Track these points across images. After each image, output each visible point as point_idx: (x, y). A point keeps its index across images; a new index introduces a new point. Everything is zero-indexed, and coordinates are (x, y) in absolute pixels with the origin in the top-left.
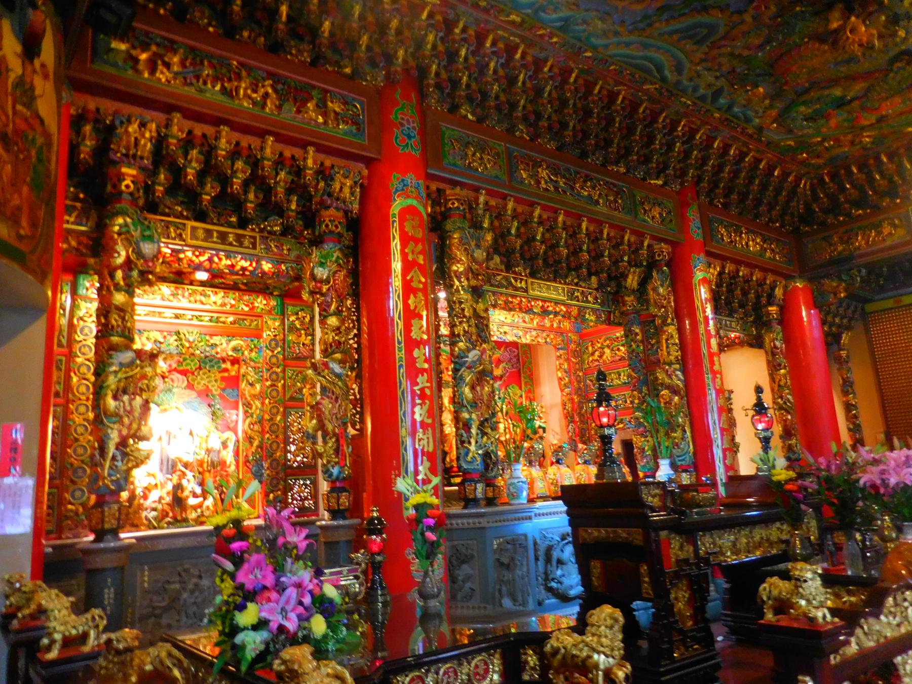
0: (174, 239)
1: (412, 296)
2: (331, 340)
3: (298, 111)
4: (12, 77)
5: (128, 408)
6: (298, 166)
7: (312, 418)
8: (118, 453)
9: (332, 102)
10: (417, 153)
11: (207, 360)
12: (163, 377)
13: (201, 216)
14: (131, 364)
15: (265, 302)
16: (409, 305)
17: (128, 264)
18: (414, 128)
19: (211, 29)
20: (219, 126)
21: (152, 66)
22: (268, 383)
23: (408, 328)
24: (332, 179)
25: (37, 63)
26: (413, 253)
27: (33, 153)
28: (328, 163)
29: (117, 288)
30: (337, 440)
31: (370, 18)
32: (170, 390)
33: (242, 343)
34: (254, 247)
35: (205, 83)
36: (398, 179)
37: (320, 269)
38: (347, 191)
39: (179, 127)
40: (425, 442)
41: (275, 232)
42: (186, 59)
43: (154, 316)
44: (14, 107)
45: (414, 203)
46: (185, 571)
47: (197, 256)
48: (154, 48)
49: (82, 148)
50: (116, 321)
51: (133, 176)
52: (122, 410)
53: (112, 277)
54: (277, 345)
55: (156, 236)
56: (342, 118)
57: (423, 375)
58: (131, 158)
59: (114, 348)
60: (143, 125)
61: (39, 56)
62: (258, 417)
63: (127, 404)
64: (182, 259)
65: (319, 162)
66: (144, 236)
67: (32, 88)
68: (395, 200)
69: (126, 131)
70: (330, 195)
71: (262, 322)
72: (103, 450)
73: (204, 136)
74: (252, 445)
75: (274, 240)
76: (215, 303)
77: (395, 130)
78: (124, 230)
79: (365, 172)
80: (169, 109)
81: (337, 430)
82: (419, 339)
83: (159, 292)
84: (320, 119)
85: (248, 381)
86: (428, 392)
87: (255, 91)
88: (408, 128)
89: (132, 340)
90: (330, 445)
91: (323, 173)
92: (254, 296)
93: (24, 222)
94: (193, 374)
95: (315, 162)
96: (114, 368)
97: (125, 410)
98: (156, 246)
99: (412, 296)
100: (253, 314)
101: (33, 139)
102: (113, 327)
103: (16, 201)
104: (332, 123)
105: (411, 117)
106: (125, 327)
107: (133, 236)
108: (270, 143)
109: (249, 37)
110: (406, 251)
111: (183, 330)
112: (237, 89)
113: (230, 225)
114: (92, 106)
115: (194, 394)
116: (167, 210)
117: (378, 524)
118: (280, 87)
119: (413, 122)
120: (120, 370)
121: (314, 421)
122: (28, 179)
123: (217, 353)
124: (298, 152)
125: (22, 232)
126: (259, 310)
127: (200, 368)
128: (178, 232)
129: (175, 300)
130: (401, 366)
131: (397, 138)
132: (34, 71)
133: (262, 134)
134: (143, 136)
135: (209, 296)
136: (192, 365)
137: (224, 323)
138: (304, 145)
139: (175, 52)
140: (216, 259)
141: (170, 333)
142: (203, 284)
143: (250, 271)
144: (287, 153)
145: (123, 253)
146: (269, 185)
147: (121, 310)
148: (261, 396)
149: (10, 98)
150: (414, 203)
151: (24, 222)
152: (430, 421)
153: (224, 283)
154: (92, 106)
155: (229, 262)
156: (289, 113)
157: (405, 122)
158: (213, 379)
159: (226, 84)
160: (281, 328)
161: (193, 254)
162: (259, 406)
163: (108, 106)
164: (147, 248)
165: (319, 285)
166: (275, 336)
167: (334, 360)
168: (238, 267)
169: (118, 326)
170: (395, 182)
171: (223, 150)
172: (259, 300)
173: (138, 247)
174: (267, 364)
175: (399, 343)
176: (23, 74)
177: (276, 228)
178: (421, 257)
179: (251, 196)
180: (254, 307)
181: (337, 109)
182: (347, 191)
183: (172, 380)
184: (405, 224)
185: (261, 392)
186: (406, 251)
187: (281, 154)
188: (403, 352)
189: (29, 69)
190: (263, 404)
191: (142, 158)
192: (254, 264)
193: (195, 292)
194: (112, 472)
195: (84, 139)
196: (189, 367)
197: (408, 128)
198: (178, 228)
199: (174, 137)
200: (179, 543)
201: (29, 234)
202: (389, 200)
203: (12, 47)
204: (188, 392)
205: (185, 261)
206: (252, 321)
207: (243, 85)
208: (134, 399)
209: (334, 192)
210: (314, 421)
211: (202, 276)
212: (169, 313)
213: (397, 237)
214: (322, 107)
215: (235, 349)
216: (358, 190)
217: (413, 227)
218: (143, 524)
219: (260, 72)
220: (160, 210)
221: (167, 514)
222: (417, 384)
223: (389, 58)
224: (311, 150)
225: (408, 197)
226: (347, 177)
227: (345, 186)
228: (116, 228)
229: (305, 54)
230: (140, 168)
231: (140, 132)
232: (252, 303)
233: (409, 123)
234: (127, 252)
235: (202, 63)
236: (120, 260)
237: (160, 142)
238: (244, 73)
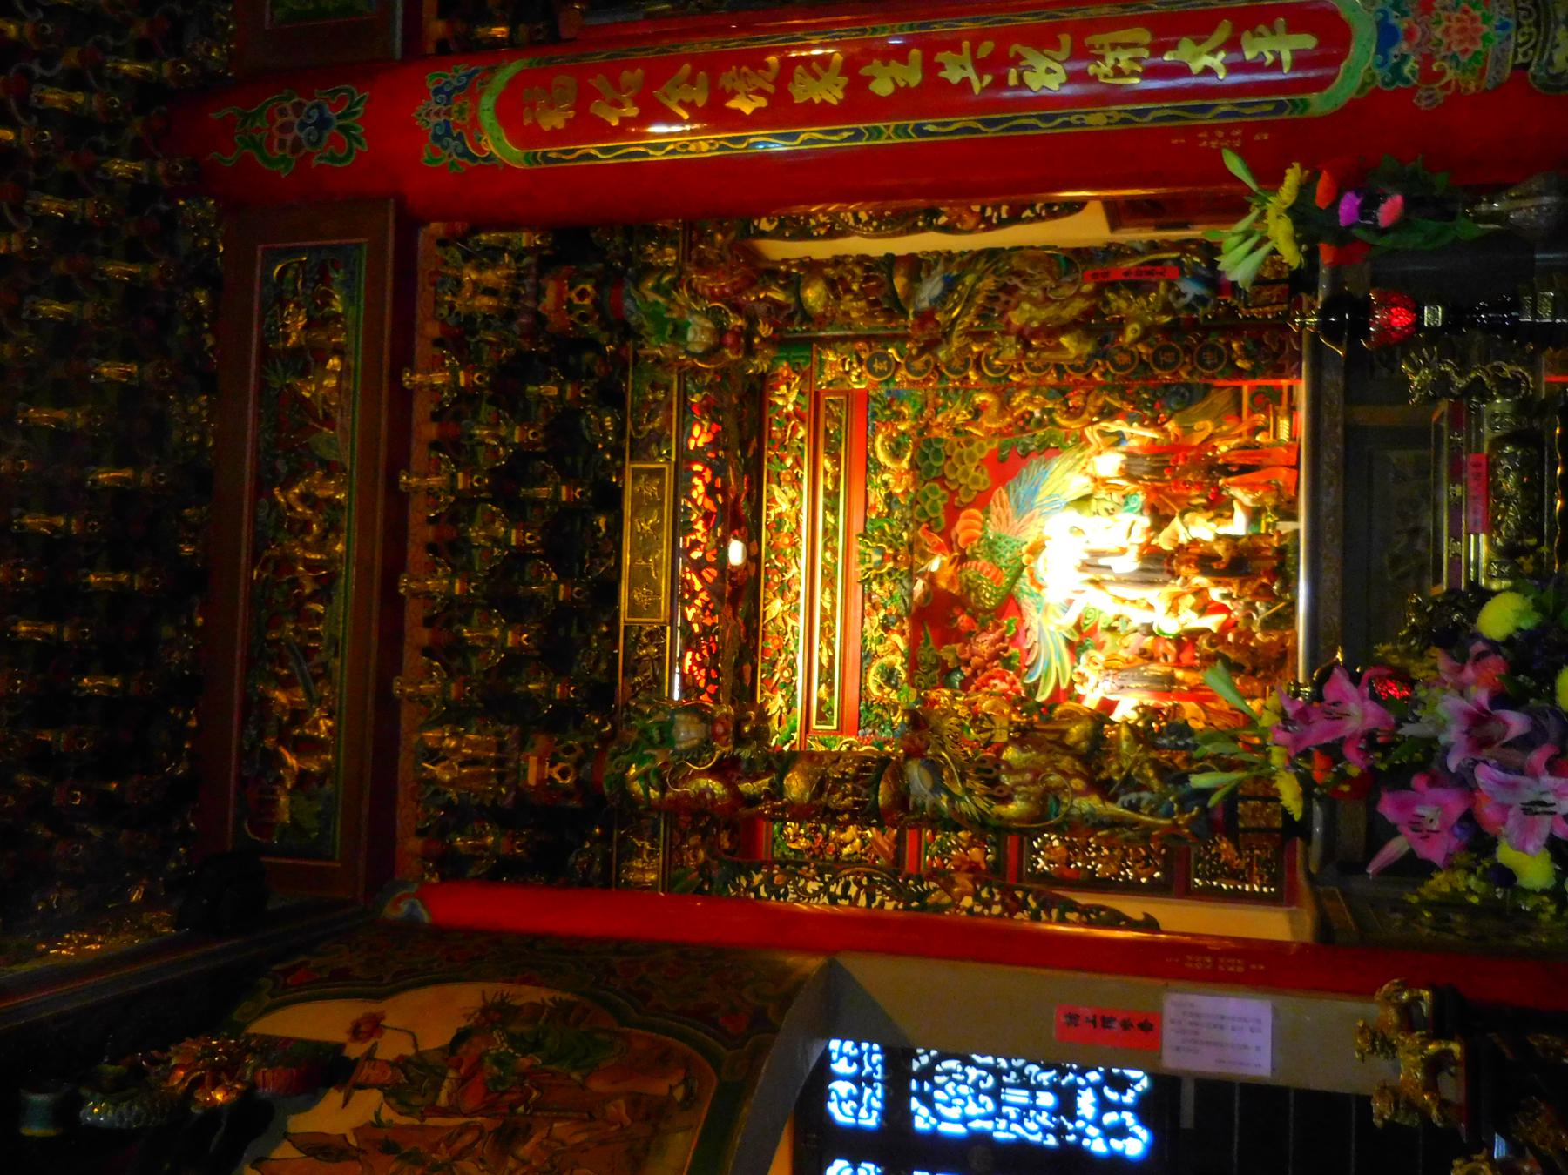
0: (662, 649)
1: (732, 104)
2: (862, 304)
3: (328, 421)
4: (388, 1114)
5: (1028, 776)
6: (455, 402)
7: (1060, 347)
8: (1123, 799)
9: (287, 337)
10: (360, 100)
11: (923, 465)
12: (963, 558)
13: (607, 591)
14: (934, 768)
15: (783, 388)
16: (757, 111)
17: (723, 770)
18: (298, 108)
19: (199, 621)
20: (402, 597)
21: (307, 746)
22: (972, 375)
23: (817, 114)
24: (470, 318)
25: (355, 1051)
26: (618, 104)
27: (524, 1062)
28: (433, 330)
29: (777, 791)
30: (1114, 287)
31: (71, 58)
32: (991, 545)
33: (880, 438)
34: (659, 473)
35: (315, 636)
36: (436, 152)
37: (690, 336)
38: (491, 277)
39: (421, 681)
40: (1124, 58)
41: (615, 423)
42: (276, 676)
43: (831, 630)
44: (444, 1112)
45: (488, 102)
46: (1396, 561)
47: (694, 595)
48: (269, 742)
49: (503, 851)
50: (844, 797)
51: (541, 762)
52: (1032, 789)
53: (753, 801)
54: (884, 357)
55: (660, 716)
56: (318, 308)
57: (941, 67)
58: (506, 768)
59: (902, 799)
60: (434, 755)
61: (341, 1047)
62: (1052, 399)
63: (1019, 779)
64: (703, 626)
65: (436, 351)
66: (662, 741)
67: (401, 1063)
68: (490, 157)
69: (452, 783)
70: (509, 316)
71: (829, 393)
72: (1114, 823)
73: (429, 622)
74: (1119, 410)
75: (636, 424)
76: (793, 502)
77: (315, 162)
78: (654, 781)
79: (437, 228)
80: (387, 705)
81: (1087, 288)
82: (844, 81)
83: (780, 622)
84: (334, 362)
85: (967, 423)
86: (986, 48)
87: (306, 526)
88: (303, 126)
89: (884, 761)
90: (1123, 304)
91: (460, 338)
92: (770, 414)
93: (660, 1088)
94: (954, 493)
95: (437, 364)
96: (944, 802)
97: (1033, 782)
98: (679, 717)
99: (732, 104)
100: (813, 411)
101: (498, 1061)
102: (856, 803)
103: (619, 1108)
104: (336, 333)
105: (272, 120)
106: (855, 779)
107: (665, 764)
108: (418, 378)
109: (192, 542)
110: (615, 123)
111: (858, 571)
112: (311, 566)
113: (616, 528)
114: (415, 844)
115: (1000, 494)
116: (603, 666)
117: (1341, 317)
118: (282, 466)
119: (283, 112)
120: (948, 792)
121: (1064, 340)
122: (576, 1076)
123: (906, 492)
124: (422, 409)
125: (679, 1094)
126: (804, 401)
127: (941, 479)
128: (645, 640)
129: (795, 588)
130: (919, 130)
131: (334, 159)
132: (369, 1056)
133: (398, 500)
134: (457, 750)
135: (780, 515)
136: (938, 498)
137: (836, 479)
138: (402, 399)
139: (266, 701)
140: (696, 555)
141: (867, 596)
142: (752, 538)
143: (714, 476)
144: (431, 431)
145: (703, 782)
146: (510, 459)
147: (821, 786)
148: (1004, 392)
149: (430, 1121)
150: (488, 102)
151: (660, 1088)
152: (1066, 40)
153: (749, 496)
154: (415, 844)
155: (699, 526)
156: (338, 442)
157: (289, 138)
158: (966, 450)
159: (308, 591)
160: (841, 348)
161: (690, 604)
162: (1025, 394)
163: (408, 814)
164: (687, 733)
165: (729, 339)
166: (860, 361)
167: (911, 293)
168: (709, 504)
169: (855, 792)
170: (440, 157)
171: (452, 584)
172: (780, 402)
173: (687, 751)
174: (927, 380)
175: (858, 135)
176: (381, 1087)
177: (608, 421)
178: (626, 76)
179: (543, 492)
180: (797, 414)
181: (302, 321)
182: (491, 277)
183: (970, 540)
184: (547, 128)
185: (994, 391)
186: (615, 123)
187: (435, 446)
188: (880, 125)
189: (366, 1072)
190: (1021, 387)
191: (501, 746)
192: (697, 468)
193: (773, 547)
194: (1162, 810)
195: (485, 847)
196: (940, 503)
197: (303, 126)
198: (638, 638)
199: (444, 691)
200: (1331, 578)
201: (680, 1075)
202: (494, 170)
203: (333, 1115)
204: (995, 509)
205: (708, 622)
206: (830, 415)
207: (298, 551)
208: (1006, 762)
209: (498, 309)
210: (1064, 340)
211: (736, 553)
212: (822, 599)
213: (585, 148)
214: (307, 360)
215: (896, 455)
216: (484, 237)
217: (551, 106)
218: (1282, 639)
219: (262, 514)
220: (604, 680)
221: (1263, 586)
222: (966, 83)
223: (140, 194)
224: (409, 379)
225: (475, 121)
226: (459, 283)
227: (477, 286)
228: (654, 794)
229: (192, 409)
230: (522, 748)
231: (449, 755)
232: (788, 417)
233: (286, 128)
234: (701, 774)
235: (276, 642)
236: (717, 787)
237: (456, 716)
238: (274, 551)
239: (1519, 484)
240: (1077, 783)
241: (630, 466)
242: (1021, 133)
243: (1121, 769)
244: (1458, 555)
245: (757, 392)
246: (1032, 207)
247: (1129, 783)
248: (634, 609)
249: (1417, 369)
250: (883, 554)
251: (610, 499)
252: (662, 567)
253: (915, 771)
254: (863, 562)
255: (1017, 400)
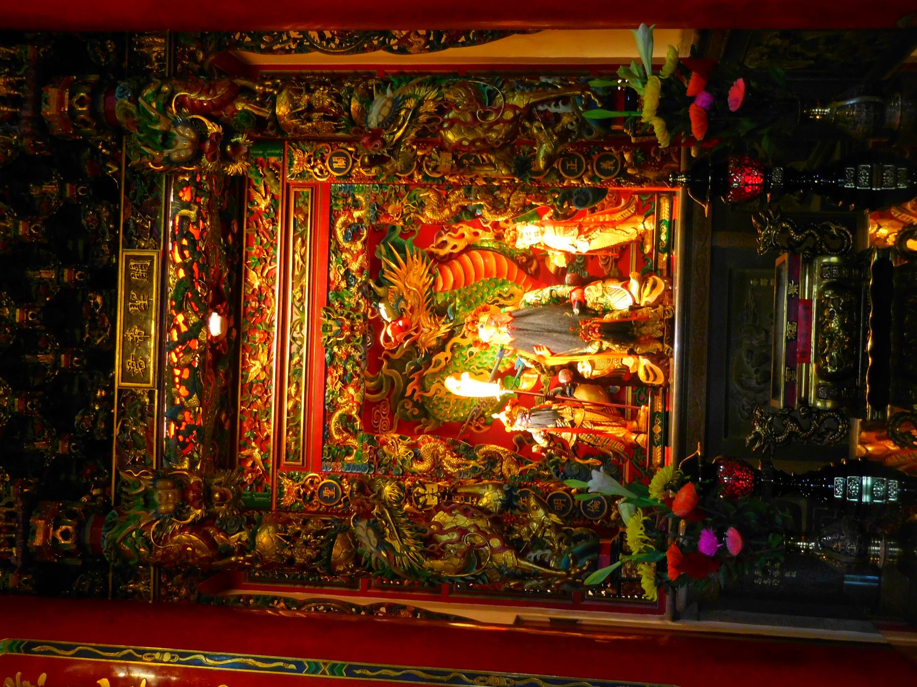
8: (532, 555)
100: (282, 203)
167: (364, 113)
239: (842, 326)
240: (496, 543)
241: (123, 254)
242: (434, 669)
243: (530, 532)
244: (794, 383)
245: (236, 192)
246: (466, 33)
247: (537, 542)
248: (126, 376)
249: (763, 225)
250: (342, 326)
251: (105, 280)
252: (150, 346)
253: (362, 530)
254: (325, 330)
255: (452, 198)
